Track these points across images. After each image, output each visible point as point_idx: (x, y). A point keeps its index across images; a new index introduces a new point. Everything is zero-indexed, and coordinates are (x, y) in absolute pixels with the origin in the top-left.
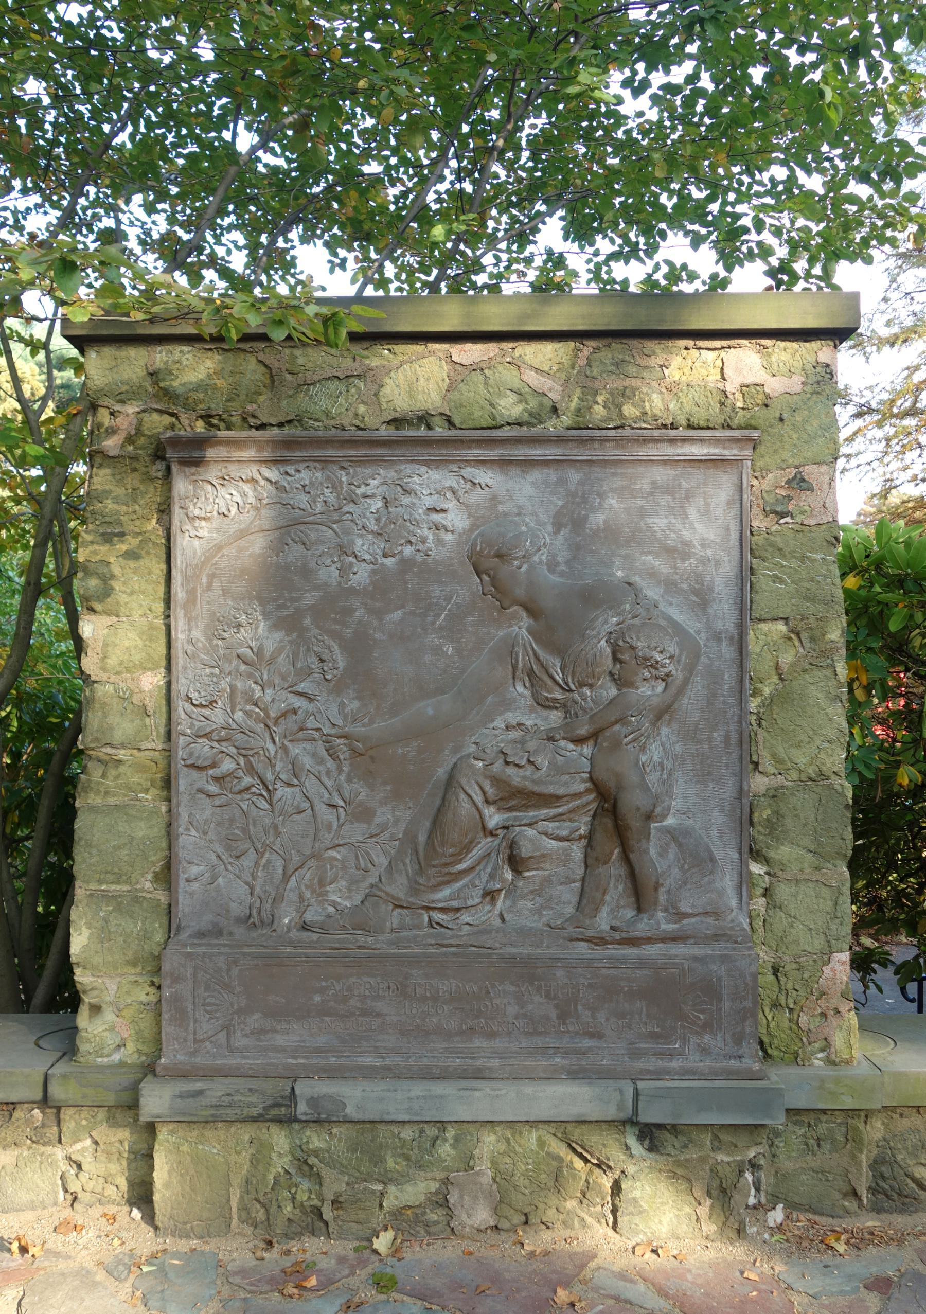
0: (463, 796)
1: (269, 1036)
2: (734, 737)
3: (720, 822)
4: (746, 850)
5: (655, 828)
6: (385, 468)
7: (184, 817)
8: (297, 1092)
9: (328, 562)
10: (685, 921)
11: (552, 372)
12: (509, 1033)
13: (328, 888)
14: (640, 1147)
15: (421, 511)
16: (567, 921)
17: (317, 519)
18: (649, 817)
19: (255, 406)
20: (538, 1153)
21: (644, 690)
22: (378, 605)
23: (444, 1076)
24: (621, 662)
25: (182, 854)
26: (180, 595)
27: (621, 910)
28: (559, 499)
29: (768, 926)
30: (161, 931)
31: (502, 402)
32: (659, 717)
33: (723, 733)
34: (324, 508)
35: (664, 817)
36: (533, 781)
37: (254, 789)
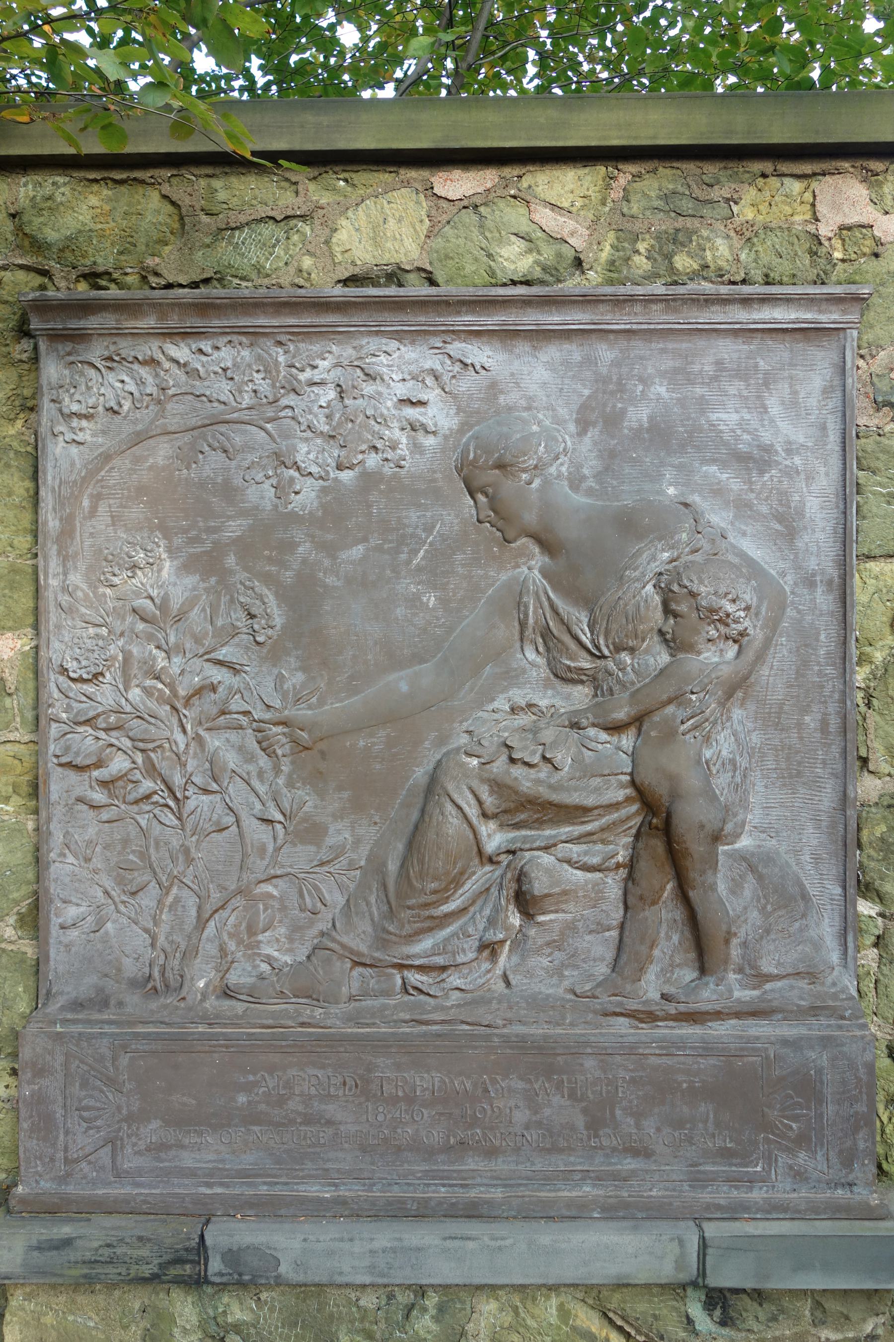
0: (449, 808)
1: (173, 1153)
2: (834, 723)
3: (815, 842)
4: (852, 882)
5: (725, 853)
6: (339, 343)
7: (58, 837)
8: (209, 1241)
9: (259, 477)
10: (768, 986)
11: (574, 209)
12: (517, 1150)
13: (260, 937)
14: (708, 1319)
15: (389, 404)
16: (599, 985)
17: (244, 416)
18: (717, 838)
19: (157, 260)
20: (559, 1328)
21: (709, 656)
22: (330, 537)
23: (422, 1213)
24: (676, 615)
25: (54, 889)
26: (51, 524)
27: (677, 970)
28: (584, 386)
29: (881, 988)
30: (26, 997)
31: (506, 252)
32: (729, 694)
33: (819, 716)
34: (254, 401)
35: (737, 836)
36: (551, 787)
37: (156, 798)
